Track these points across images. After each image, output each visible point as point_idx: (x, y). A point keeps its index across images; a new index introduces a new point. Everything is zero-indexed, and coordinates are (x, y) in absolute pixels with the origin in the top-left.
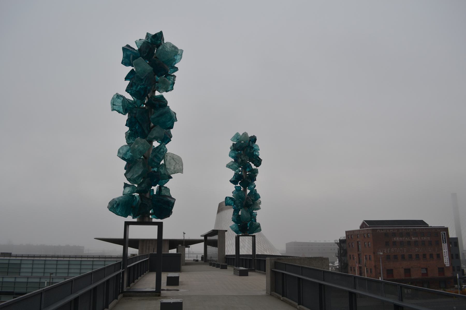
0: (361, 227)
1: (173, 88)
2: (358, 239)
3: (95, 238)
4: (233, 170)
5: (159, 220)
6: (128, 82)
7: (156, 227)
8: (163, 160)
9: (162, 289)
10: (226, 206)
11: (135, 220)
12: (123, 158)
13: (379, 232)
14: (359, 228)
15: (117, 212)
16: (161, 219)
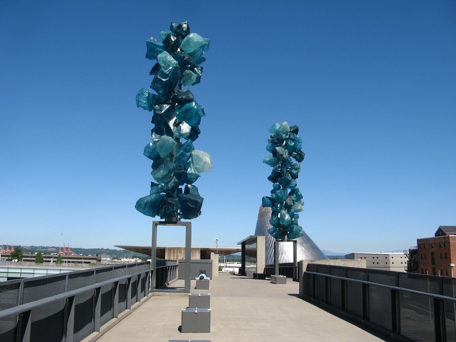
0: (437, 234)
1: (200, 80)
2: (433, 249)
3: (114, 246)
4: (271, 167)
5: (187, 220)
7: (184, 227)
8: (191, 158)
9: (263, 273)
10: (263, 207)
11: (163, 220)
12: (150, 157)
16: (189, 219)
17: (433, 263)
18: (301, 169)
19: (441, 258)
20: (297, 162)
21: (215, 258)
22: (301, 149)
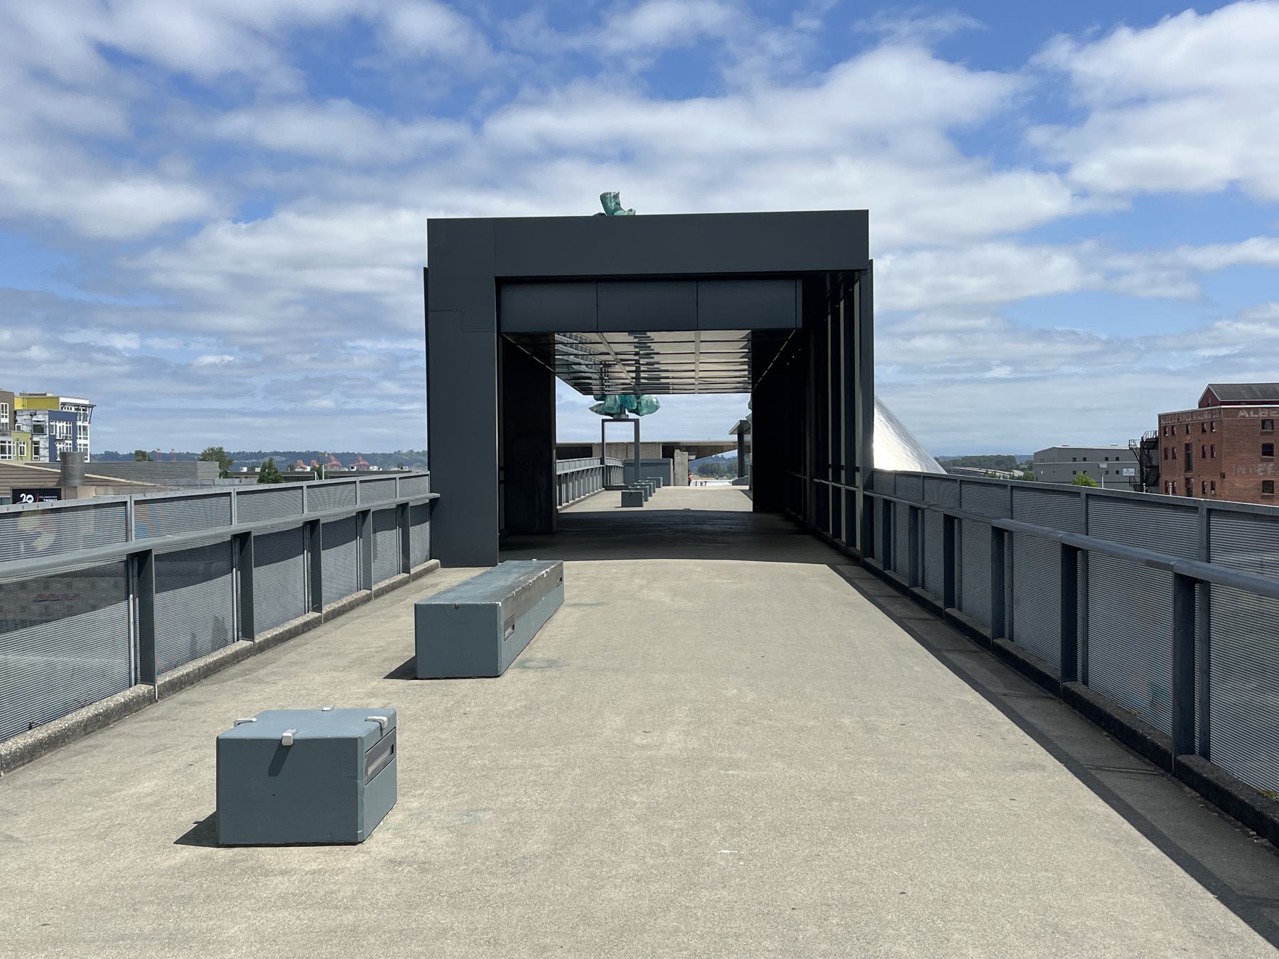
2: (1188, 438)
6: (870, 259)
9: (559, 441)
13: (1244, 416)
14: (1196, 407)
15: (79, 441)
17: (1188, 467)
19: (1204, 456)
21: (680, 457)
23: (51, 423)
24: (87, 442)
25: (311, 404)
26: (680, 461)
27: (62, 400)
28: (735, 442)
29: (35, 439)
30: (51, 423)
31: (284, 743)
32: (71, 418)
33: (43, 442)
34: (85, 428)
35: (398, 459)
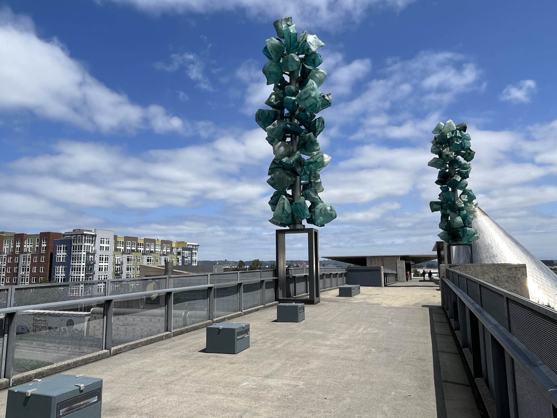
15: (193, 258)
18: (471, 168)
20: (465, 162)
22: (470, 147)
23: (183, 252)
24: (196, 258)
25: (296, 246)
26: (400, 266)
27: (188, 243)
28: (436, 255)
29: (178, 257)
30: (183, 252)
31: (220, 329)
32: (191, 250)
33: (180, 258)
34: (196, 253)
35: (301, 262)
